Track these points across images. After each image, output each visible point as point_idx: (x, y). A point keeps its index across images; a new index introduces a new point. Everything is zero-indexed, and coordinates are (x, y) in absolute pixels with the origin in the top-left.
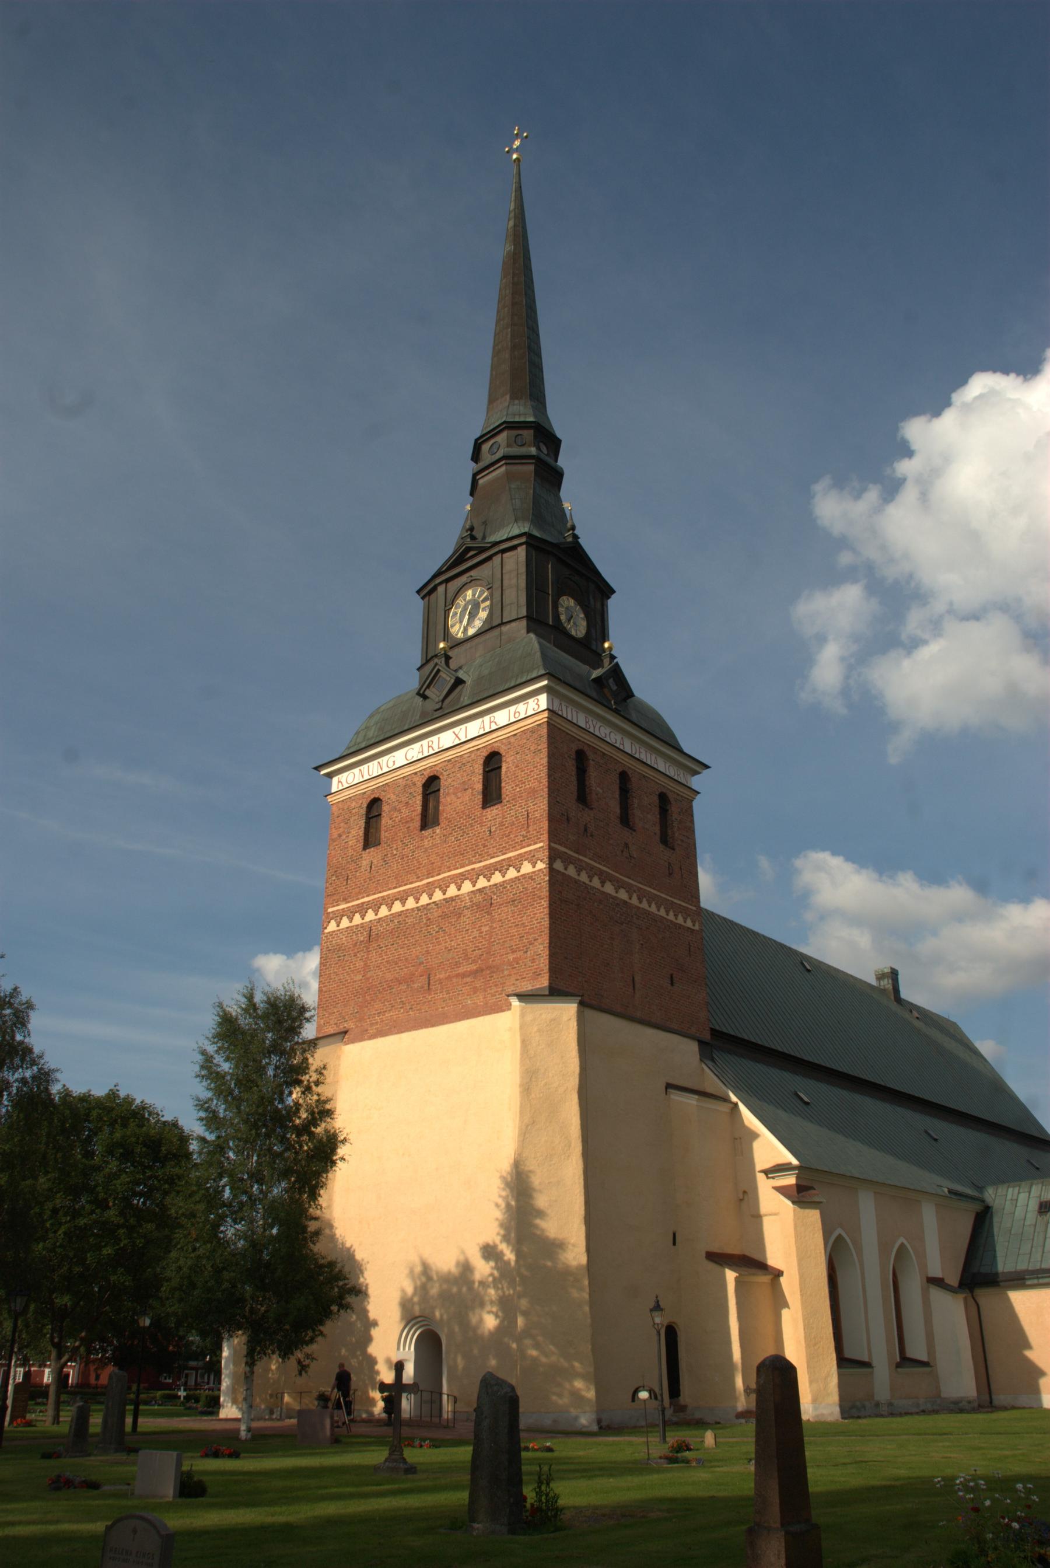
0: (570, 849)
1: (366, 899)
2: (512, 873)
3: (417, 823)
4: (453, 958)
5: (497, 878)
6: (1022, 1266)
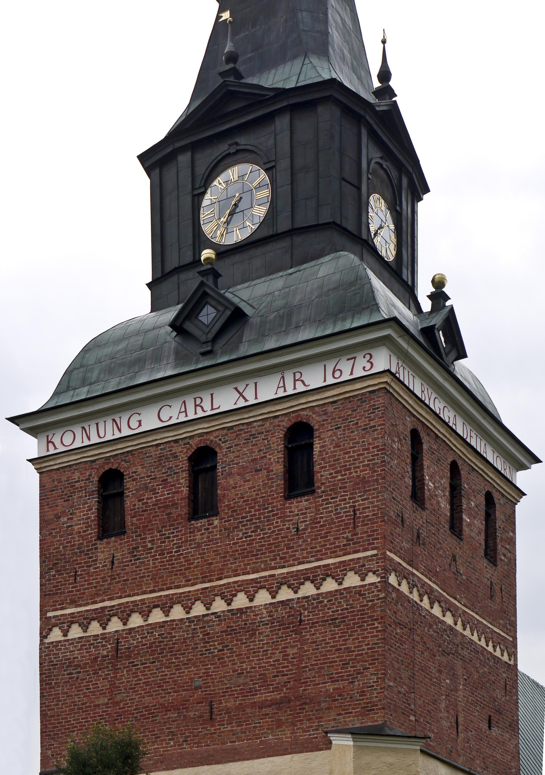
0: (404, 560)
1: (107, 604)
2: (330, 585)
3: (183, 510)
4: (245, 684)
5: (308, 589)
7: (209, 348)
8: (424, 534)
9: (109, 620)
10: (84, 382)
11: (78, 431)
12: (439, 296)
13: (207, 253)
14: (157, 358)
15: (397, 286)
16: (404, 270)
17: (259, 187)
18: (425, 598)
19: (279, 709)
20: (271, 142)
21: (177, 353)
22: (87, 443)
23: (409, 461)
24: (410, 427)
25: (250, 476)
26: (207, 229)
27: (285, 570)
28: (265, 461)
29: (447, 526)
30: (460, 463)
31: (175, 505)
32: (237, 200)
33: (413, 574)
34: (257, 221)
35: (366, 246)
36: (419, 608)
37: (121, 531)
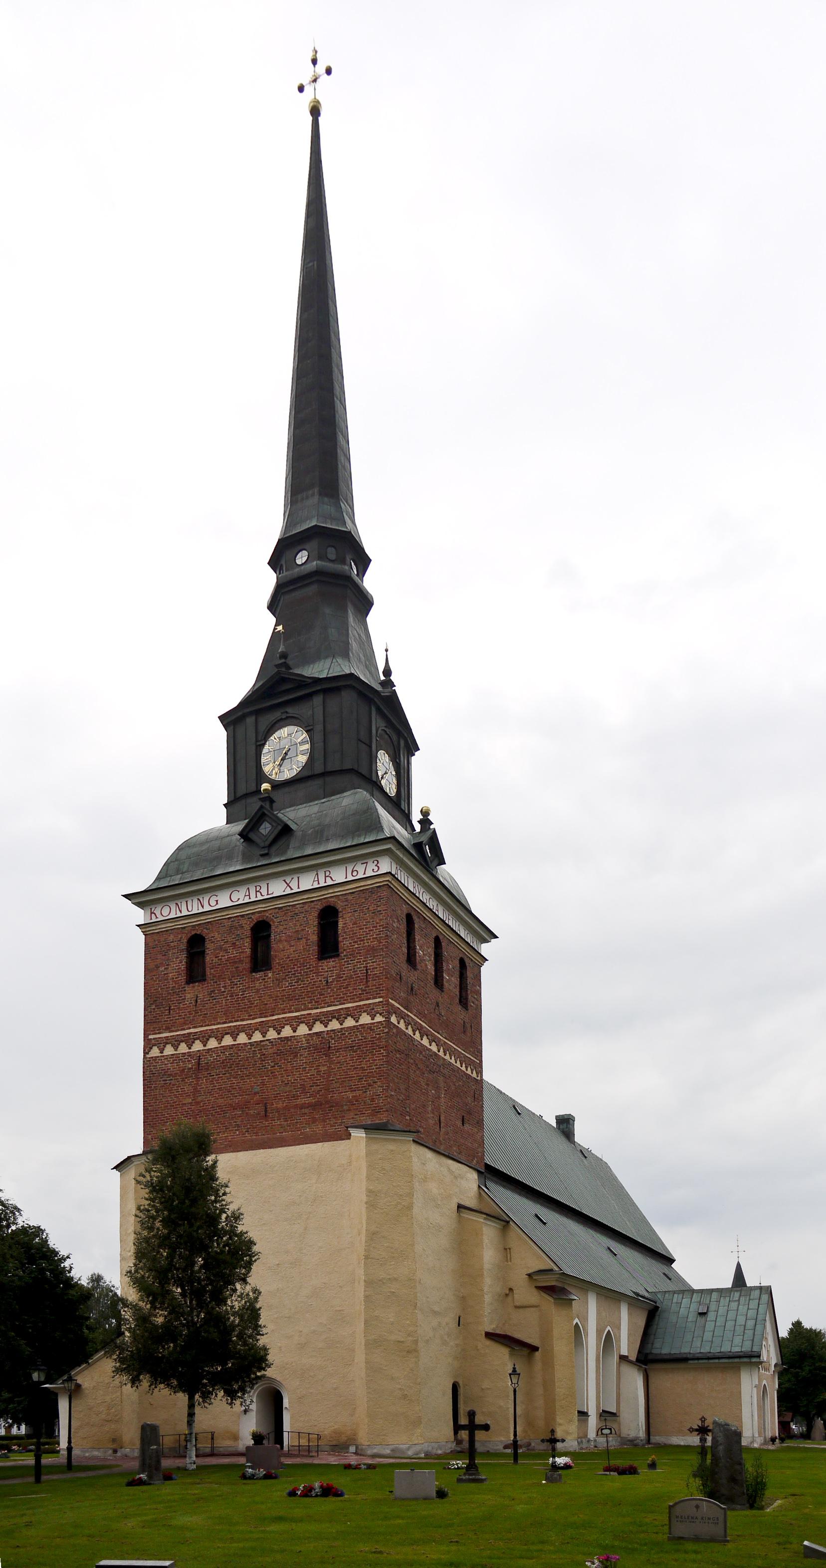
2: (350, 1022)
3: (246, 964)
4: (290, 1091)
5: (334, 1025)
6: (685, 1350)
7: (266, 852)
8: (416, 987)
9: (193, 1042)
10: (178, 871)
11: (173, 907)
12: (425, 822)
13: (265, 786)
14: (230, 857)
15: (397, 813)
16: (403, 803)
17: (302, 743)
18: (417, 1033)
19: (314, 1109)
20: (310, 712)
21: (244, 854)
22: (179, 915)
23: (405, 935)
24: (405, 912)
25: (294, 943)
26: (267, 769)
27: (318, 1011)
28: (304, 932)
29: (432, 982)
30: (441, 937)
31: (241, 961)
32: (287, 751)
33: (408, 1016)
34: (301, 765)
35: (375, 786)
36: (412, 1039)
37: (202, 978)
